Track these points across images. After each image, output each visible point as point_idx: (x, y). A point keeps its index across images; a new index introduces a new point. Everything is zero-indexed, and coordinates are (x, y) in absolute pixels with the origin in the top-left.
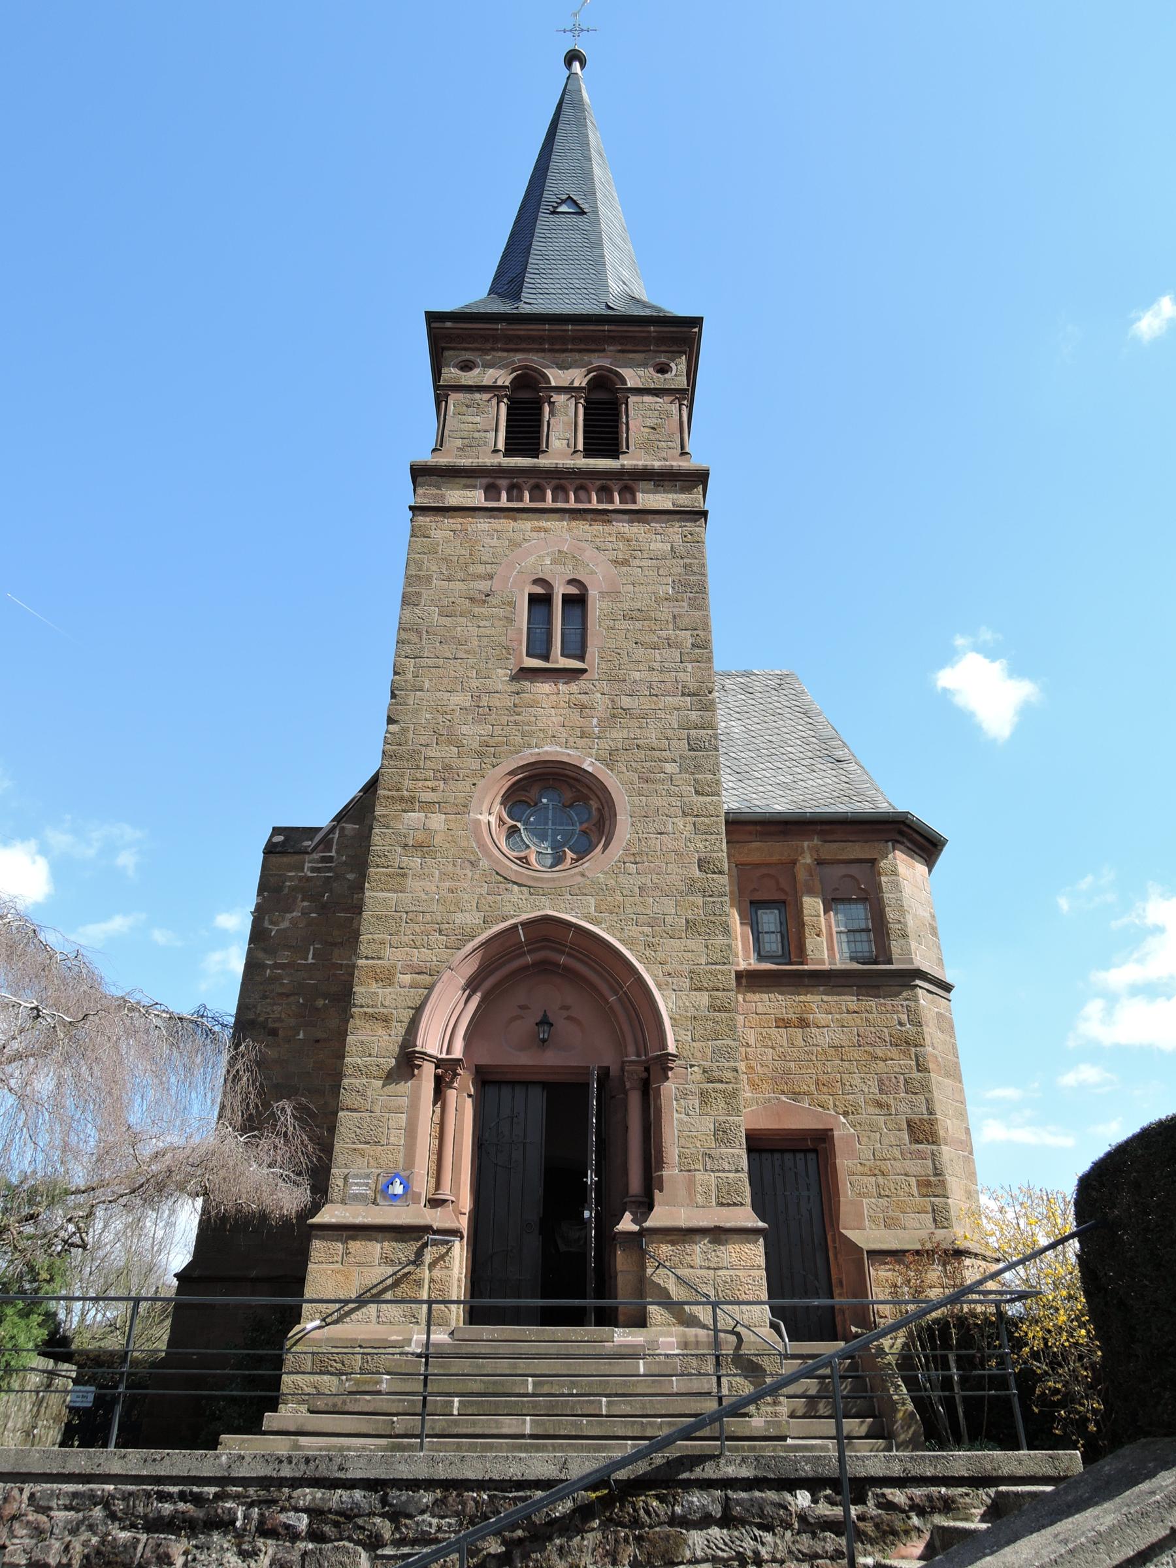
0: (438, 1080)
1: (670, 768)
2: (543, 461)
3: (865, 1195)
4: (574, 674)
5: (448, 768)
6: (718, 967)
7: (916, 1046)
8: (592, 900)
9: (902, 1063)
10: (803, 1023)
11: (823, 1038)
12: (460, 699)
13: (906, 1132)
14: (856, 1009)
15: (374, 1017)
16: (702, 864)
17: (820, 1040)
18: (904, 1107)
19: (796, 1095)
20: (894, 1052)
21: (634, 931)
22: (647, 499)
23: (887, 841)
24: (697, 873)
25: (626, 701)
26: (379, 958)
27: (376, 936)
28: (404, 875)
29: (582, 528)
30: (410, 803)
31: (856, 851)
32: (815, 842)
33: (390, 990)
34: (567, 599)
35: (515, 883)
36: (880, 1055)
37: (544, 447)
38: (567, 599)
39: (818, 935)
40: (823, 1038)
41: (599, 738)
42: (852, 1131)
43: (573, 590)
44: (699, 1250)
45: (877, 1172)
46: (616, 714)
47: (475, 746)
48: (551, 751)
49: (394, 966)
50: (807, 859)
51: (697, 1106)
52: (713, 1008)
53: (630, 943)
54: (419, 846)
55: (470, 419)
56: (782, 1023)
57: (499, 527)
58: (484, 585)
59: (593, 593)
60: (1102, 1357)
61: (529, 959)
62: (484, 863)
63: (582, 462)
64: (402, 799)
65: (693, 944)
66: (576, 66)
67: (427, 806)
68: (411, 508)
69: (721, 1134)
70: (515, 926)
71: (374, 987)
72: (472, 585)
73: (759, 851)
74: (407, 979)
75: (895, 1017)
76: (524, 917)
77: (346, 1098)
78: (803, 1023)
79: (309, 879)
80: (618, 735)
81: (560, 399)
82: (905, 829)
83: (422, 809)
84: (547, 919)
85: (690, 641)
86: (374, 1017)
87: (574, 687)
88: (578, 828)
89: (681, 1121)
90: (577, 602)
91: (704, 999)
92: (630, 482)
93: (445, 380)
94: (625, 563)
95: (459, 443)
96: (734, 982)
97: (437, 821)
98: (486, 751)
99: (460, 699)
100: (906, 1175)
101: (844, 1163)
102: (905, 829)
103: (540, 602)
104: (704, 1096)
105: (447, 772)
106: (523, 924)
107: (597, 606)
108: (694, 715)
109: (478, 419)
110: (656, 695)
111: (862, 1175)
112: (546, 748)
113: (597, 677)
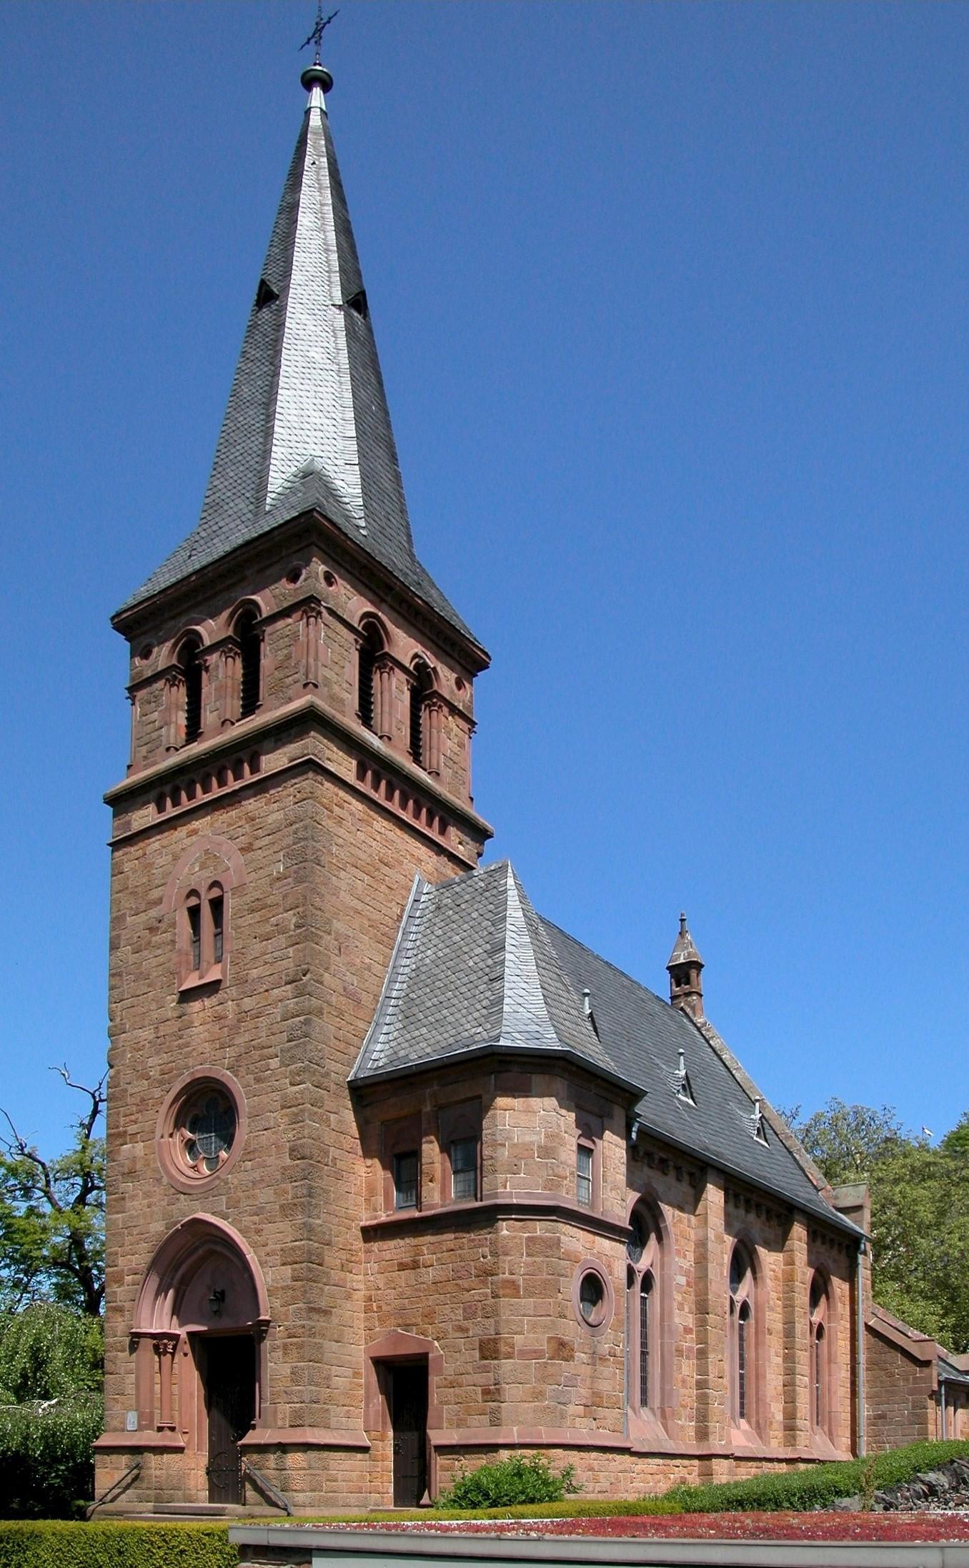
3: (447, 1403)
6: (297, 1243)
7: (493, 1275)
11: (430, 1275)
13: (477, 1351)
18: (479, 1328)
19: (407, 1326)
21: (247, 1221)
24: (288, 1162)
26: (116, 1266)
28: (123, 1199)
33: (122, 1288)
35: (182, 1193)
36: (466, 1286)
39: (431, 1181)
40: (430, 1275)
41: (229, 1046)
42: (442, 1352)
43: (216, 892)
44: (272, 1459)
45: (455, 1385)
46: (242, 1016)
49: (123, 1271)
51: (281, 1357)
52: (295, 1279)
56: (402, 1267)
57: (165, 842)
62: (165, 1180)
68: (110, 845)
74: (128, 1279)
75: (480, 1251)
85: (294, 920)
87: (214, 1000)
89: (271, 1367)
100: (474, 1385)
104: (285, 1347)
110: (267, 991)
111: (445, 1387)
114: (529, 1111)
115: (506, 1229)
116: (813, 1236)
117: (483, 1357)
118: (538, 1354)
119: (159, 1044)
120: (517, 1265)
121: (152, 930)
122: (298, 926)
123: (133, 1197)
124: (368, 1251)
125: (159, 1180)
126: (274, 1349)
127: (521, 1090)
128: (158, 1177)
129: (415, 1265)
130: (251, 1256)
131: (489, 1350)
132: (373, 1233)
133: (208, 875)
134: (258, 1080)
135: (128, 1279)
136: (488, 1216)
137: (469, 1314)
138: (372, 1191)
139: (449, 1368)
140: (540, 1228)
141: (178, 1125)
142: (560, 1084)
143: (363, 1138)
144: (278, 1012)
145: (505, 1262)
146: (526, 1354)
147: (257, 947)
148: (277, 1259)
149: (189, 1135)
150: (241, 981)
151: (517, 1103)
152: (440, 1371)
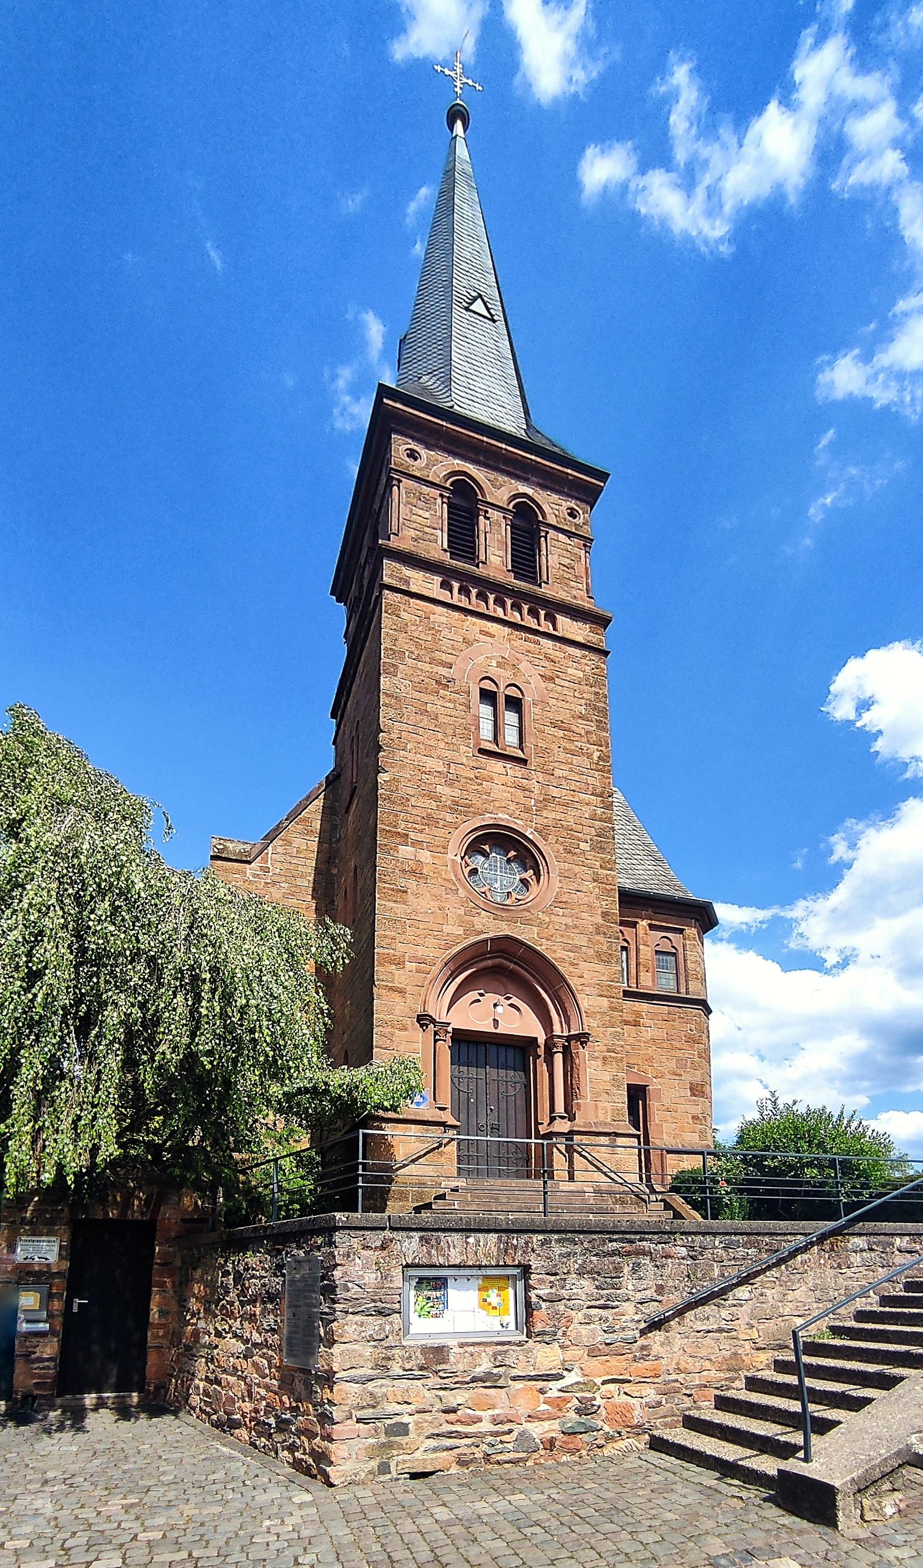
1: (583, 846)
2: (482, 571)
5: (429, 817)
8: (535, 929)
9: (691, 1053)
11: (648, 1034)
14: (666, 1018)
16: (605, 915)
17: (644, 1034)
20: (686, 1046)
22: (566, 626)
23: (692, 919)
25: (555, 792)
27: (387, 933)
29: (520, 641)
32: (650, 912)
37: (482, 558)
40: (648, 1034)
47: (449, 803)
48: (503, 818)
55: (421, 512)
58: (443, 671)
59: (528, 699)
60: (107, 1220)
61: (490, 963)
63: (511, 579)
66: (459, 125)
67: (415, 843)
69: (615, 1080)
70: (485, 941)
72: (436, 669)
76: (491, 935)
78: (637, 1024)
81: (495, 515)
82: (704, 913)
83: (413, 845)
84: (507, 938)
88: (518, 877)
91: (605, 1002)
92: (553, 611)
93: (395, 464)
94: (551, 679)
95: (412, 533)
96: (622, 994)
97: (425, 856)
102: (704, 913)
105: (430, 820)
106: (491, 939)
107: (531, 711)
108: (599, 811)
109: (427, 515)
112: (500, 815)
113: (533, 768)
128: (453, 888)
152: (659, 1100)
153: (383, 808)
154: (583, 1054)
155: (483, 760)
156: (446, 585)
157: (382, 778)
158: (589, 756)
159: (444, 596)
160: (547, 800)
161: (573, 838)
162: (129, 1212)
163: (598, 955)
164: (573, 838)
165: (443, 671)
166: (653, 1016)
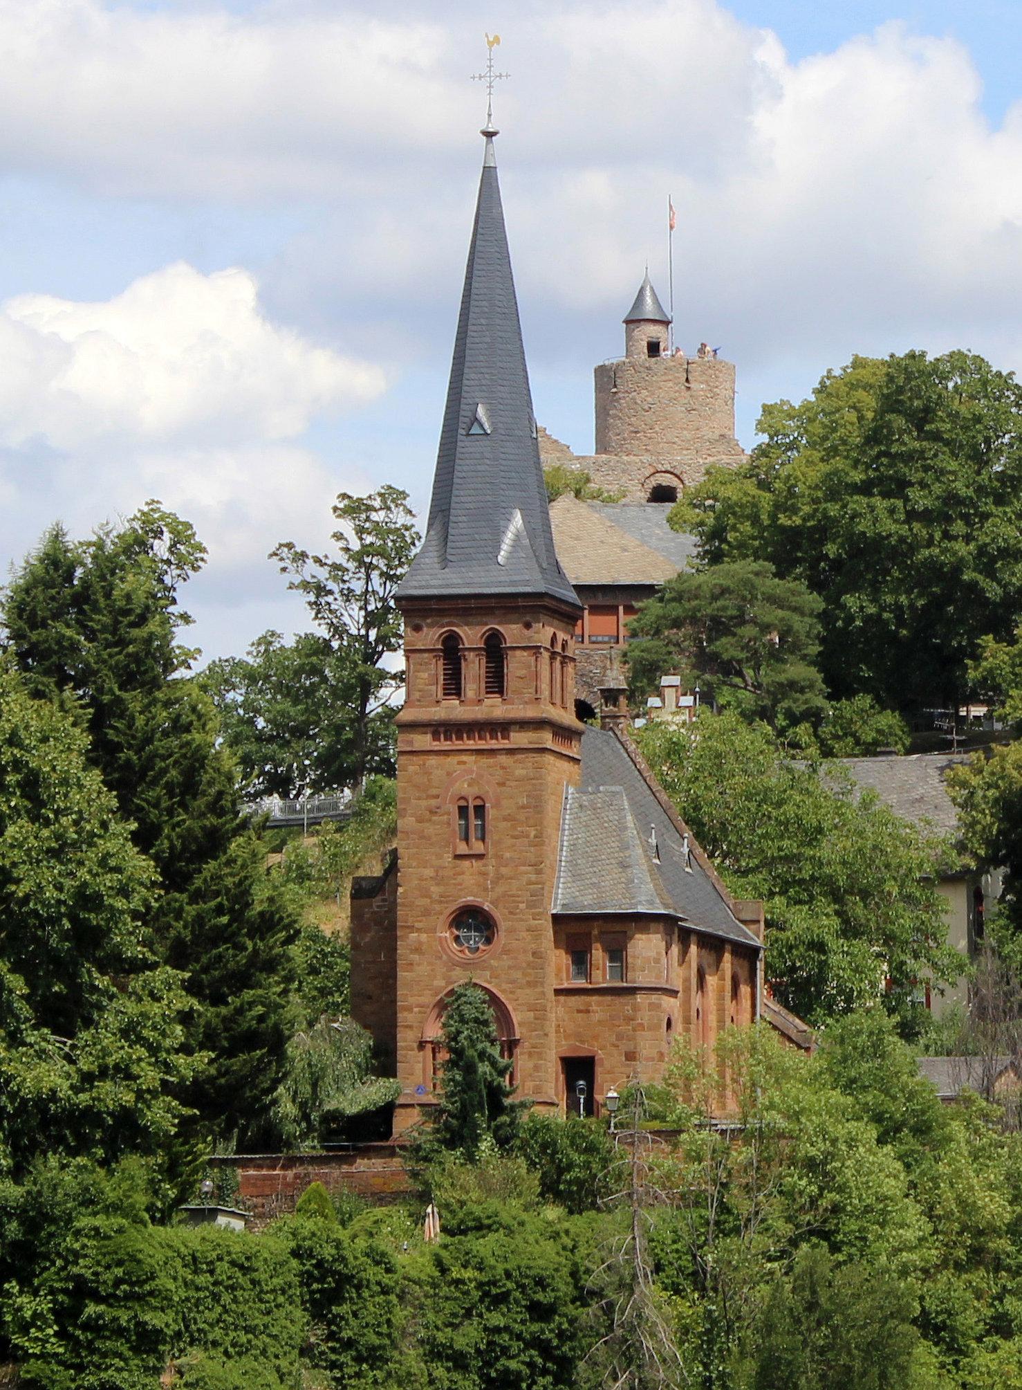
0: (433, 1049)
4: (480, 857)
10: (588, 1011)
11: (596, 1017)
12: (429, 872)
15: (407, 1027)
18: (625, 1046)
19: (582, 1042)
21: (504, 986)
30: (412, 928)
31: (618, 927)
34: (475, 807)
38: (475, 807)
43: (479, 803)
46: (499, 878)
50: (595, 932)
53: (503, 991)
54: (417, 950)
56: (579, 1011)
62: (445, 957)
64: (408, 927)
65: (528, 991)
67: (419, 930)
71: (406, 1014)
73: (574, 928)
74: (416, 1010)
77: (399, 1058)
79: (376, 913)
80: (500, 890)
81: (471, 656)
86: (407, 1027)
90: (480, 811)
97: (424, 937)
98: (443, 900)
99: (429, 872)
101: (598, 1070)
103: (463, 811)
105: (426, 913)
107: (491, 813)
114: (650, 940)
115: (639, 998)
116: (734, 953)
117: (627, 1059)
118: (652, 1059)
119: (438, 880)
120: (644, 1017)
121: (432, 812)
122: (536, 837)
123: (419, 965)
124: (557, 1001)
125: (441, 958)
126: (522, 1054)
127: (645, 930)
129: (588, 1011)
130: (510, 1008)
131: (631, 1056)
132: (558, 992)
133: (475, 791)
134: (511, 913)
135: (416, 1010)
136: (632, 991)
137: (620, 1037)
138: (559, 970)
139: (607, 1064)
140: (654, 998)
141: (450, 926)
142: (661, 927)
143: (556, 941)
144: (524, 879)
145: (639, 1014)
146: (648, 1059)
147: (510, 841)
148: (525, 1008)
149: (457, 933)
150: (498, 857)
151: (644, 937)
152: (602, 1065)
153: (400, 913)
154: (517, 1051)
155: (458, 862)
156: (436, 737)
157: (400, 890)
158: (528, 836)
159: (436, 746)
160: (499, 878)
161: (514, 902)
162: (223, 1081)
163: (528, 982)
164: (514, 902)
165: (433, 802)
166: (599, 1004)
